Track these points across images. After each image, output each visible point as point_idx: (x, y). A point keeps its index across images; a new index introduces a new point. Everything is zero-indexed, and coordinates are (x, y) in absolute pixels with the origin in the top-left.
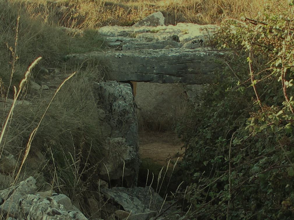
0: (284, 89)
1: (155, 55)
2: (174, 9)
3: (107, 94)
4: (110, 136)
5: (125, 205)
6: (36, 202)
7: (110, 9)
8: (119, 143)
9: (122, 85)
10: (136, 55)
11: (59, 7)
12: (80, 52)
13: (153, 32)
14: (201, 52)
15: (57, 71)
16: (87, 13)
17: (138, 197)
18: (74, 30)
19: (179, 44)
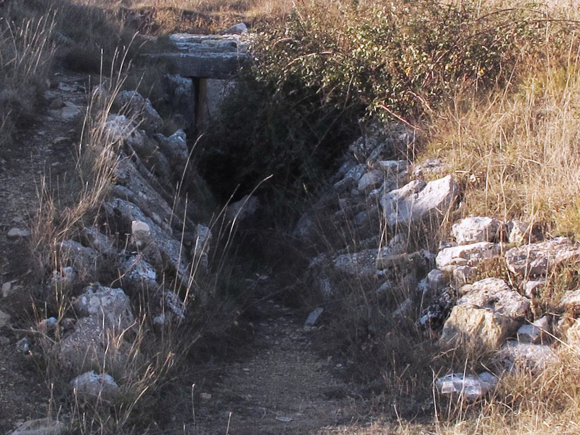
7: (190, 19)
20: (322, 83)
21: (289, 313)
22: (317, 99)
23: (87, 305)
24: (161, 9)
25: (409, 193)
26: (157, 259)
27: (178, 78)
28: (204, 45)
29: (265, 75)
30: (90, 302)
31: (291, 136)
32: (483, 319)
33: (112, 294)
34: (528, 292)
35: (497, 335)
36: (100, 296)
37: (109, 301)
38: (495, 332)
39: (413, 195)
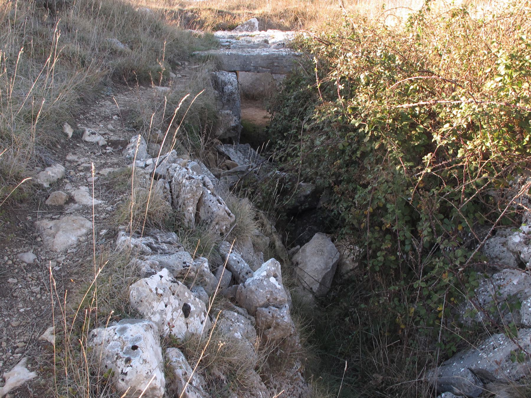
0: (338, 90)
1: (252, 53)
2: (265, 16)
3: (220, 81)
4: (222, 109)
5: (231, 157)
6: (178, 170)
7: (222, 16)
8: (228, 114)
9: (230, 74)
10: (240, 53)
11: (187, 13)
12: (202, 50)
13: (251, 36)
14: (284, 52)
15: (186, 63)
16: (205, 18)
17: (240, 151)
18: (197, 32)
19: (268, 45)
24: (204, 10)
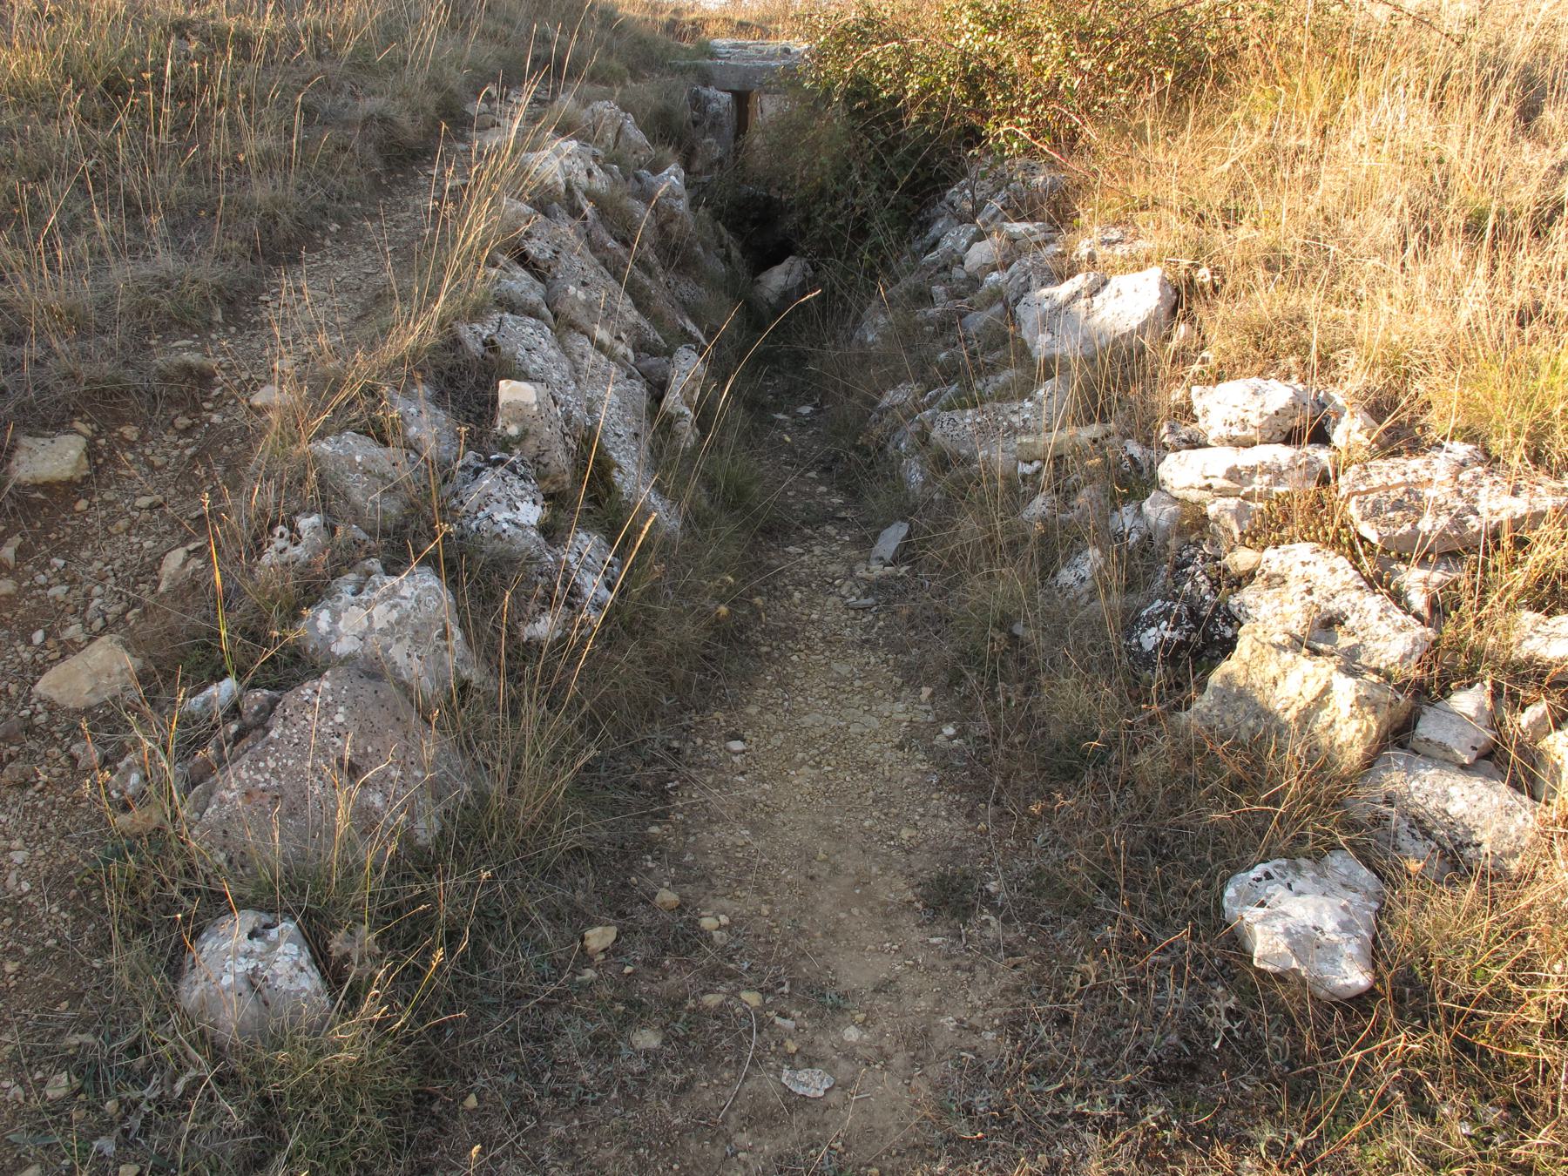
20: (905, 92)
21: (843, 514)
22: (896, 116)
23: (330, 633)
25: (1075, 296)
26: (553, 463)
27: (711, 92)
28: (750, 52)
29: (817, 80)
30: (341, 624)
31: (856, 176)
32: (1326, 690)
33: (402, 593)
34: (1419, 601)
35: (1365, 737)
36: (368, 605)
37: (395, 615)
38: (1359, 730)
39: (1082, 302)
